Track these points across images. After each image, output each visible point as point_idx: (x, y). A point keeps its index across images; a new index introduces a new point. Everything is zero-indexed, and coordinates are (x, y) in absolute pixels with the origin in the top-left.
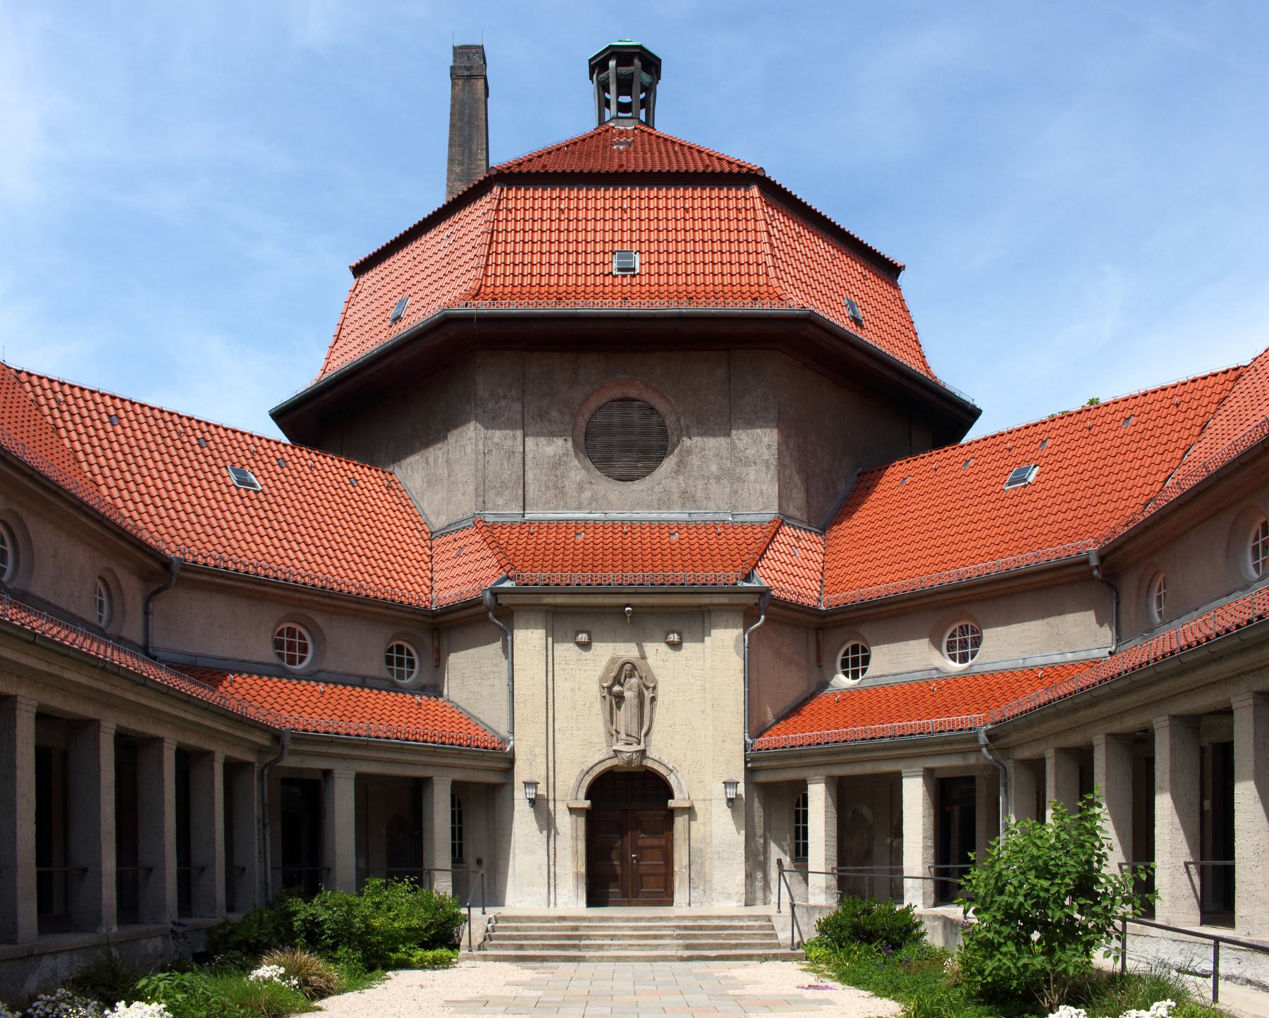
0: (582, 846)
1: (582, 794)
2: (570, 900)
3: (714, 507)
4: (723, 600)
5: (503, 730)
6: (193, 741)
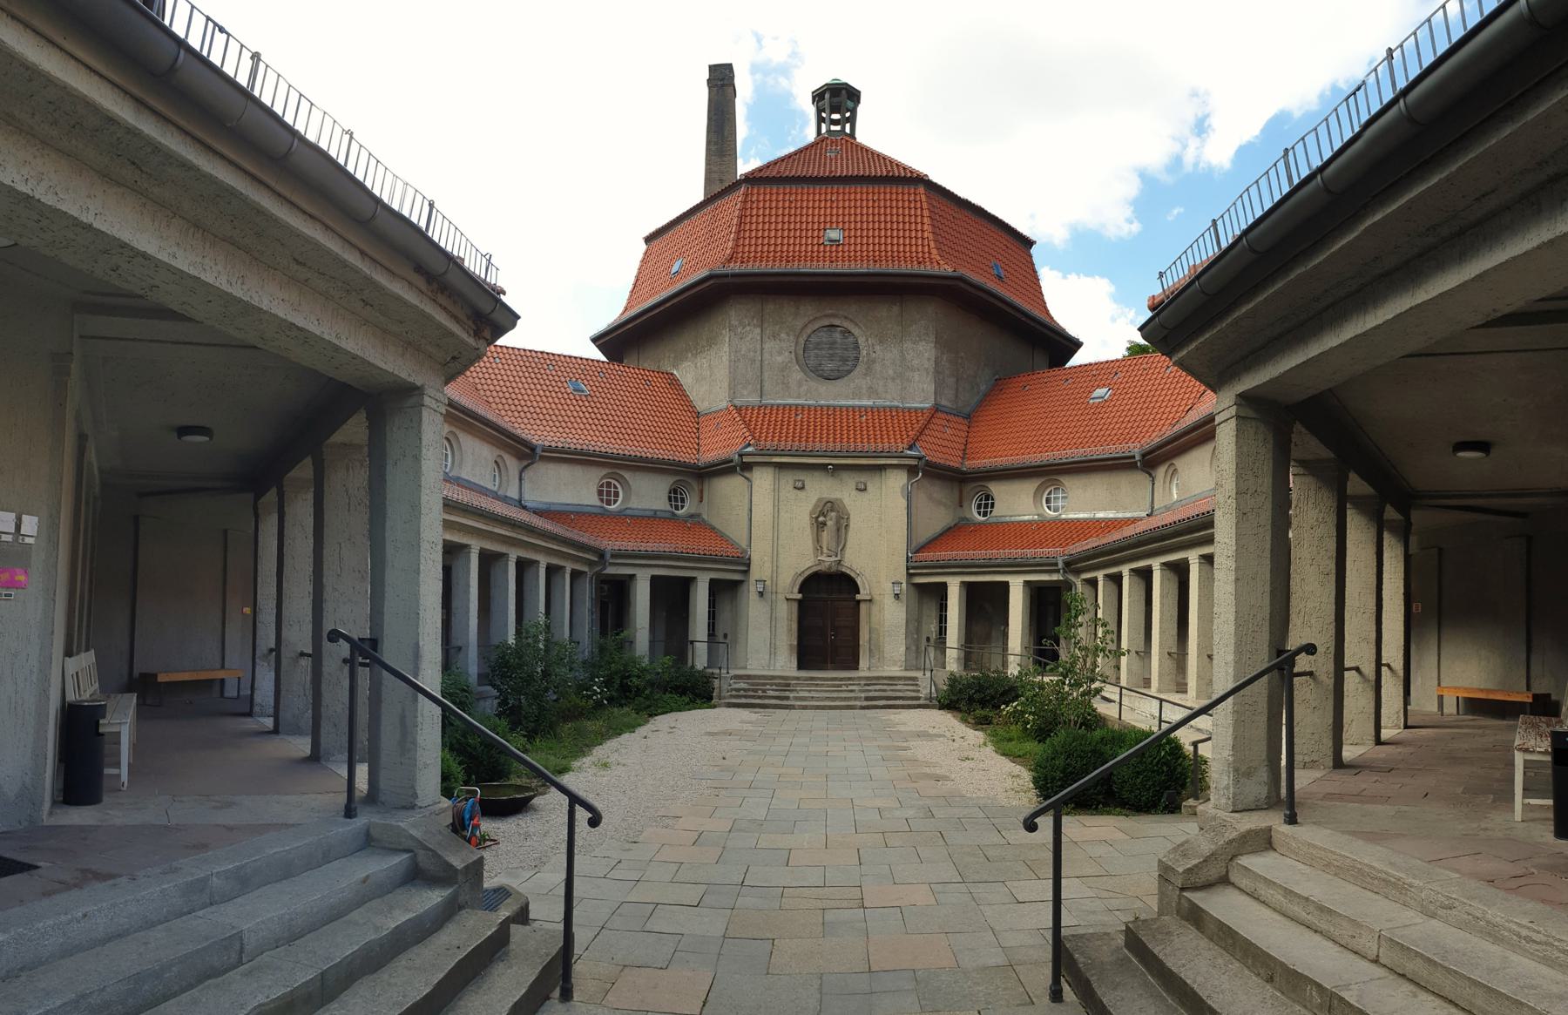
0: (795, 626)
1: (796, 589)
2: (785, 664)
3: (890, 398)
4: (895, 462)
5: (744, 545)
6: (555, 561)
